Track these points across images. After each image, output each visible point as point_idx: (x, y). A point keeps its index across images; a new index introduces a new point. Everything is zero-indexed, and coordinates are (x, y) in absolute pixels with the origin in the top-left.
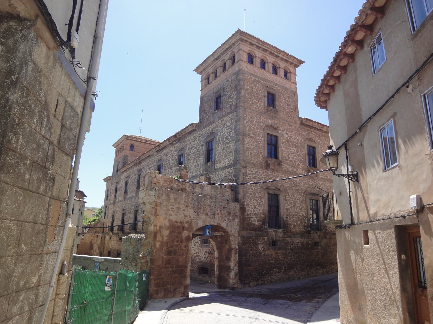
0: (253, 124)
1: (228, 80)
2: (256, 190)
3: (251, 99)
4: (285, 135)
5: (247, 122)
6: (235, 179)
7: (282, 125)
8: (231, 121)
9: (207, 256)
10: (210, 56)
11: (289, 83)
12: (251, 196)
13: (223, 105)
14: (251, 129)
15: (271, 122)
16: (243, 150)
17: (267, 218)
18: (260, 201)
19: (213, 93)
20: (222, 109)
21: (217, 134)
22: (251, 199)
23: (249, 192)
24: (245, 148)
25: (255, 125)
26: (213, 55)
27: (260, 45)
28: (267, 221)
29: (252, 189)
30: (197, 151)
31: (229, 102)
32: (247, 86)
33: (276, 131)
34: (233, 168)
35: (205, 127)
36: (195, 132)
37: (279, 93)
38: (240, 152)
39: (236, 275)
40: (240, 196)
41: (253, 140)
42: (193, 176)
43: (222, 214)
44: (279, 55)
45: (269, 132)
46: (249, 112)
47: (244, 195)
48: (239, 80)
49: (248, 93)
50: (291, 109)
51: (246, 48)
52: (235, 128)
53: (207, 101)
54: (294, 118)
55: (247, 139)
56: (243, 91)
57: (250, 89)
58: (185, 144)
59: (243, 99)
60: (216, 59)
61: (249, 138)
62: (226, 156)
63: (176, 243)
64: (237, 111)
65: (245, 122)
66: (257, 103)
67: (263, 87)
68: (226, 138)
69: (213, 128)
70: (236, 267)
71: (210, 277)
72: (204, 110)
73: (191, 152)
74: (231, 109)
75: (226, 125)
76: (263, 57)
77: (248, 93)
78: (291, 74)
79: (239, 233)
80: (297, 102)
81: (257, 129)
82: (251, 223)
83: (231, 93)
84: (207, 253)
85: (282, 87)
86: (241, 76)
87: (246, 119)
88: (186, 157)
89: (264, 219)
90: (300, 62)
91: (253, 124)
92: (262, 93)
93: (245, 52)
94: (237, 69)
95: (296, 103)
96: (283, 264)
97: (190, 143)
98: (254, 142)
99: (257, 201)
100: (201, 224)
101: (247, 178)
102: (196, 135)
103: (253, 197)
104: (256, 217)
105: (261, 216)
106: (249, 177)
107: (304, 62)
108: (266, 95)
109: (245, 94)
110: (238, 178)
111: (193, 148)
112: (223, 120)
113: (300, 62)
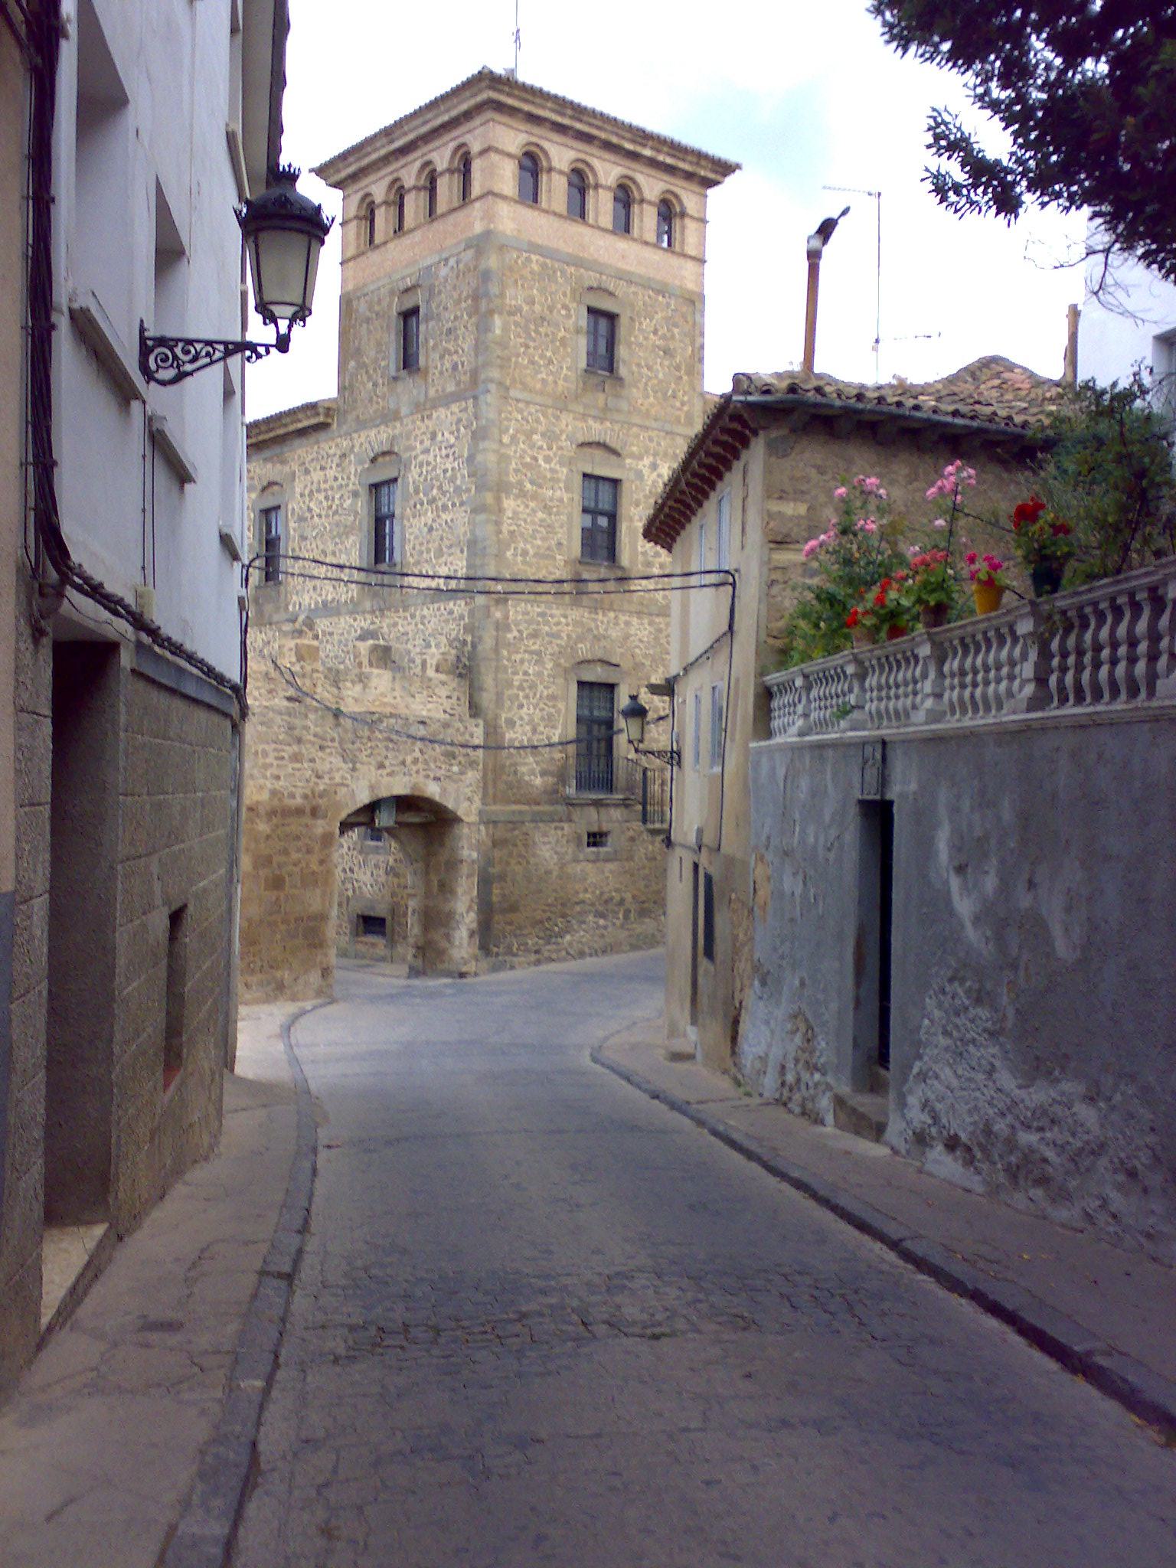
0: (532, 446)
1: (446, 260)
2: (539, 674)
3: (527, 347)
4: (646, 472)
5: (513, 438)
6: (469, 639)
7: (638, 436)
8: (458, 430)
9: (383, 879)
10: (376, 135)
11: (675, 261)
12: (521, 694)
13: (427, 357)
14: (525, 465)
15: (596, 430)
16: (499, 541)
17: (572, 761)
18: (552, 710)
19: (392, 293)
20: (427, 368)
21: (407, 467)
22: (521, 706)
23: (516, 683)
24: (505, 534)
25: (541, 448)
26: (387, 133)
27: (566, 121)
28: (573, 773)
29: (526, 673)
30: (336, 512)
31: (447, 351)
32: (514, 297)
33: (613, 458)
34: (463, 603)
35: (362, 425)
36: (322, 435)
37: (632, 305)
38: (488, 551)
39: (472, 934)
40: (486, 699)
41: (532, 504)
42: (325, 603)
43: (426, 762)
44: (639, 149)
45: (589, 471)
46: (518, 401)
47: (499, 696)
48: (486, 276)
49: (517, 324)
50: (678, 368)
51: (512, 138)
52: (471, 459)
53: (368, 320)
54: (683, 404)
55: (509, 504)
56: (498, 321)
57: (526, 308)
58: (287, 469)
59: (499, 353)
60: (404, 151)
61: (517, 497)
62: (440, 553)
63: (295, 856)
64: (475, 398)
65: (506, 439)
66: (550, 362)
67: (574, 291)
68: (440, 488)
69: (394, 437)
70: (472, 915)
71: (392, 944)
72: (358, 352)
73: (310, 510)
74: (458, 384)
75: (439, 437)
76: (580, 166)
77: (517, 324)
78: (687, 221)
79: (480, 813)
80: (702, 334)
81: (547, 460)
82: (519, 782)
83: (456, 318)
84: (382, 872)
85: (646, 284)
86: (492, 262)
87: (507, 430)
88: (292, 524)
89: (565, 767)
90: (725, 169)
91: (532, 446)
92: (569, 316)
93: (509, 155)
94: (478, 228)
95: (699, 341)
96: (622, 902)
97: (307, 472)
98: (534, 511)
99: (542, 710)
100: (364, 798)
101: (510, 636)
102: (329, 446)
103: (527, 697)
104: (537, 763)
105: (552, 759)
106: (516, 633)
107: (738, 167)
108: (583, 320)
109: (505, 329)
110: (480, 638)
111: (321, 497)
112: (429, 417)
113: (725, 169)
